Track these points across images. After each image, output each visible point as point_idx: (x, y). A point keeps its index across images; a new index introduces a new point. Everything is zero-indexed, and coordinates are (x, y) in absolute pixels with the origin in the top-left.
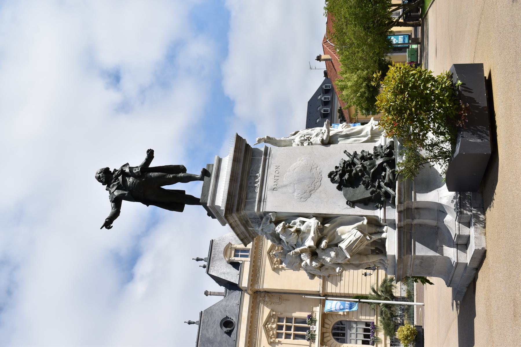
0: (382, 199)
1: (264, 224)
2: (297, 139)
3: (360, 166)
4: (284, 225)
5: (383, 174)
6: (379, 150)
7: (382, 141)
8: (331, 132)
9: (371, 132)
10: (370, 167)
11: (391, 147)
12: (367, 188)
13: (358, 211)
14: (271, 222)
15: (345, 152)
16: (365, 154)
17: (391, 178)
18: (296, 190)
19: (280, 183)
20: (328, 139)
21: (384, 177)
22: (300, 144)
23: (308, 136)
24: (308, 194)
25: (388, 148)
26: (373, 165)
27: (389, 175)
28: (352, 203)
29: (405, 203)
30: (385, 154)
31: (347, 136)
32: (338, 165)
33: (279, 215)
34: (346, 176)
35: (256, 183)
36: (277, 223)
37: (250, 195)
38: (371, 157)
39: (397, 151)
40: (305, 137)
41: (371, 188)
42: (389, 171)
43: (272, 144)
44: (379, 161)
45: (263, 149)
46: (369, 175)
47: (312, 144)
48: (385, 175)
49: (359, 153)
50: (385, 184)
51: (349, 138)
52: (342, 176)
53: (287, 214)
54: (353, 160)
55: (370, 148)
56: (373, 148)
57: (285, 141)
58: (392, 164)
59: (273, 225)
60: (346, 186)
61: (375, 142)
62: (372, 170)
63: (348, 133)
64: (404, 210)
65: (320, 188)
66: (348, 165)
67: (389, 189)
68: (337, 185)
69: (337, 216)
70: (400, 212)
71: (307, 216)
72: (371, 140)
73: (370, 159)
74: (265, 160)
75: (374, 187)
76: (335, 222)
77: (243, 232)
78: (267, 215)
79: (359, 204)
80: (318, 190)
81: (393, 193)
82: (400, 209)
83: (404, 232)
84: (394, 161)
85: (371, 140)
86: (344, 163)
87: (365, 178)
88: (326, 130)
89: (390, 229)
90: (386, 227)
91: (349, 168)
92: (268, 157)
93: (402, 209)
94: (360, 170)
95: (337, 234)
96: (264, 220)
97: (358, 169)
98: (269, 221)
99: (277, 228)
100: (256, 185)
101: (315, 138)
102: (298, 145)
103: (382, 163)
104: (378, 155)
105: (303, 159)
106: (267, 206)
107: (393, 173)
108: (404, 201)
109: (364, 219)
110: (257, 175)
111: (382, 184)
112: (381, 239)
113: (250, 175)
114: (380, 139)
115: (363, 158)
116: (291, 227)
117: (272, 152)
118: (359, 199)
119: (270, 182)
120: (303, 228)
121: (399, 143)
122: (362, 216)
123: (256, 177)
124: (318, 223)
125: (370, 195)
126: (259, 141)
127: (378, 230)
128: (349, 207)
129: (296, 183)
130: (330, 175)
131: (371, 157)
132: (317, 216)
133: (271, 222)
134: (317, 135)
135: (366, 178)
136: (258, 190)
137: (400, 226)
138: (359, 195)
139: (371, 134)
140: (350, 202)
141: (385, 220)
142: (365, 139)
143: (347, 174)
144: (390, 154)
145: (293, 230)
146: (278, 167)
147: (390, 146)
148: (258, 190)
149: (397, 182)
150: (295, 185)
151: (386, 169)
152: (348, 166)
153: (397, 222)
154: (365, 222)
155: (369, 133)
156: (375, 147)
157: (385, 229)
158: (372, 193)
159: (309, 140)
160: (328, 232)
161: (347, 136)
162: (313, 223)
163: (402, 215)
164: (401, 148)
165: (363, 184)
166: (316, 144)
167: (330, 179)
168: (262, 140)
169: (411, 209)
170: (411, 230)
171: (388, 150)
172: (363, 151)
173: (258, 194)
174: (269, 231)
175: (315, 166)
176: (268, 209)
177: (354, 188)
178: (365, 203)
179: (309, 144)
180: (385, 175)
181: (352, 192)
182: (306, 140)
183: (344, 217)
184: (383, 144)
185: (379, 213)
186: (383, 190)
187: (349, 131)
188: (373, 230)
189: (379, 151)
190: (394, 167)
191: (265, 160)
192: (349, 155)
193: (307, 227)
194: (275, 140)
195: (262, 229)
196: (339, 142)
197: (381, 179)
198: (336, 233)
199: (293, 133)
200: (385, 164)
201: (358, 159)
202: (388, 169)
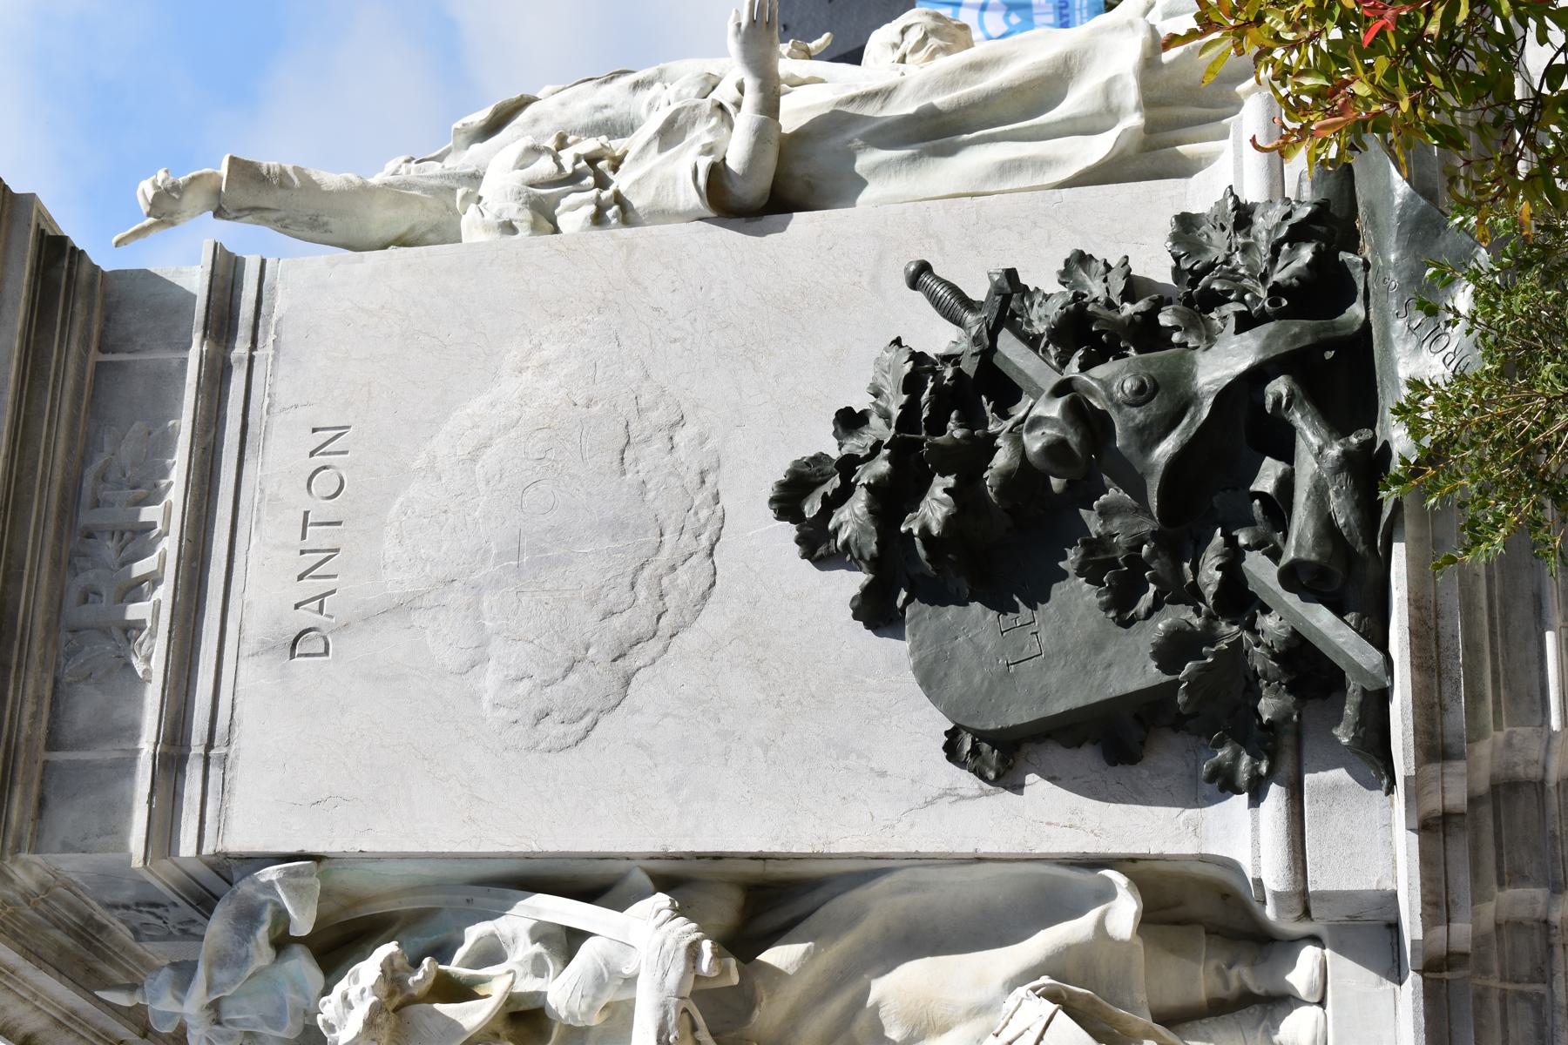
0: (1268, 707)
1: (222, 960)
2: (502, 168)
3: (1054, 409)
4: (392, 977)
5: (1266, 480)
6: (1218, 245)
7: (1242, 164)
8: (785, 102)
9: (1144, 86)
10: (1139, 416)
11: (1332, 223)
12: (1121, 604)
13: (1052, 817)
14: (282, 943)
15: (914, 282)
16: (1096, 288)
17: (1341, 512)
18: (496, 648)
19: (351, 587)
20: (770, 162)
21: (1279, 507)
22: (523, 218)
23: (589, 145)
24: (602, 673)
25: (1298, 234)
26: (1166, 396)
27: (1319, 493)
28: (996, 753)
29: (1484, 749)
30: (1276, 291)
31: (934, 132)
32: (860, 401)
33: (349, 879)
34: (935, 508)
35: (134, 590)
36: (336, 946)
37: (85, 708)
38: (1150, 316)
39: (1382, 254)
40: (567, 157)
41: (1157, 605)
42: (1315, 450)
43: (284, 226)
44: (1223, 361)
45: (195, 280)
46: (1136, 487)
47: (627, 215)
48: (1286, 484)
49: (1042, 276)
50: (1291, 577)
51: (952, 151)
52: (893, 500)
53: (427, 871)
54: (988, 353)
55: (1137, 235)
56: (1167, 226)
57: (397, 192)
58: (1341, 378)
59: (302, 966)
60: (937, 595)
61: (1184, 169)
62: (1167, 447)
63: (941, 100)
64: (1473, 801)
65: (712, 620)
66: (946, 399)
67: (1321, 620)
68: (853, 581)
69: (867, 872)
70: (1434, 828)
71: (597, 884)
72: (1150, 158)
73: (1147, 334)
74: (216, 377)
75: (1192, 595)
76: (852, 921)
77: (71, 1015)
78: (244, 887)
79: (1055, 754)
80: (687, 639)
81: (1368, 657)
82: (1434, 804)
83: (1481, 997)
84: (1359, 353)
85: (1150, 158)
86: (912, 384)
87: (1106, 513)
88: (751, 84)
89: (1352, 978)
90: (1308, 956)
91: (954, 430)
92: (240, 349)
93: (1457, 797)
94: (1055, 450)
95: (878, 1029)
96: (217, 927)
97: (1034, 443)
98: (263, 933)
99: (329, 1008)
100: (136, 611)
101: (654, 159)
102: (509, 228)
103: (1256, 377)
104: (1214, 300)
105: (550, 351)
106: (238, 805)
107: (1367, 468)
108: (1476, 733)
109: (1106, 894)
110: (148, 514)
111: (1261, 570)
112: (1337, 343)
113: (86, 518)
114: (1226, 145)
115: (1081, 332)
116: (462, 991)
117: (280, 304)
118: (1058, 707)
119: (262, 581)
120: (563, 992)
121: (1400, 187)
122: (1095, 863)
123: (140, 538)
124: (693, 952)
125: (1150, 675)
126: (166, 207)
127: (1244, 976)
128: (966, 780)
129: (497, 583)
130: (788, 500)
131: (1150, 316)
132: (678, 879)
133: (282, 943)
134: (670, 133)
135: (1113, 518)
136: (152, 660)
137: (1439, 947)
138: (1053, 678)
139: (1149, 102)
140: (980, 736)
141: (1303, 900)
142: (1098, 148)
143: (940, 486)
144: (1325, 289)
145: (471, 1016)
146: (328, 439)
147: (1321, 211)
148: (152, 660)
149: (1399, 551)
150: (487, 600)
151: (1290, 432)
152: (946, 405)
153: (1412, 928)
154: (1123, 913)
155: (1130, 94)
156: (1186, 224)
157: (1302, 972)
158: (1172, 651)
159: (602, 182)
160: (796, 1018)
161: (934, 132)
162: (647, 945)
163: (1459, 851)
164: (1423, 228)
165: (1091, 571)
166: (662, 215)
167: (789, 530)
168: (192, 199)
169: (1540, 785)
170: (1543, 974)
171: (1306, 253)
172: (1081, 259)
173: (153, 696)
174: (276, 1023)
175: (657, 416)
176: (240, 839)
177: (1003, 606)
178: (1110, 743)
179: (598, 219)
180: (1286, 484)
181: (989, 641)
182: (575, 178)
183: (930, 874)
184: (1253, 192)
185: (1241, 835)
186: (1269, 623)
187: (950, 81)
188: (1198, 977)
189: (1217, 252)
190: (1369, 417)
191: (216, 377)
192: (953, 304)
193: (600, 983)
194: (310, 186)
195: (215, 1006)
196: (862, 184)
197: (1249, 522)
198: (861, 1024)
199: (480, 116)
200: (1279, 387)
201: (1032, 342)
202: (1308, 435)
